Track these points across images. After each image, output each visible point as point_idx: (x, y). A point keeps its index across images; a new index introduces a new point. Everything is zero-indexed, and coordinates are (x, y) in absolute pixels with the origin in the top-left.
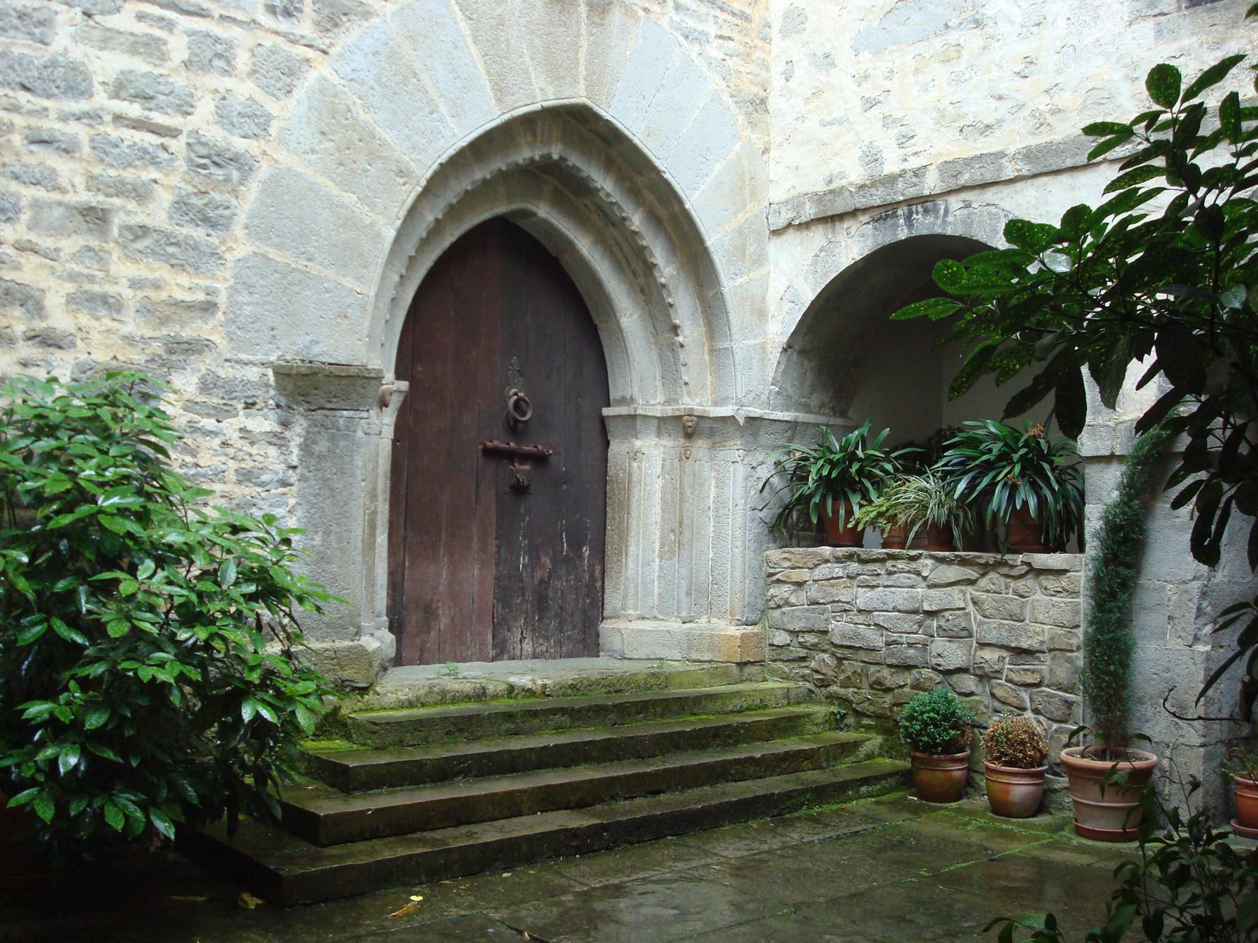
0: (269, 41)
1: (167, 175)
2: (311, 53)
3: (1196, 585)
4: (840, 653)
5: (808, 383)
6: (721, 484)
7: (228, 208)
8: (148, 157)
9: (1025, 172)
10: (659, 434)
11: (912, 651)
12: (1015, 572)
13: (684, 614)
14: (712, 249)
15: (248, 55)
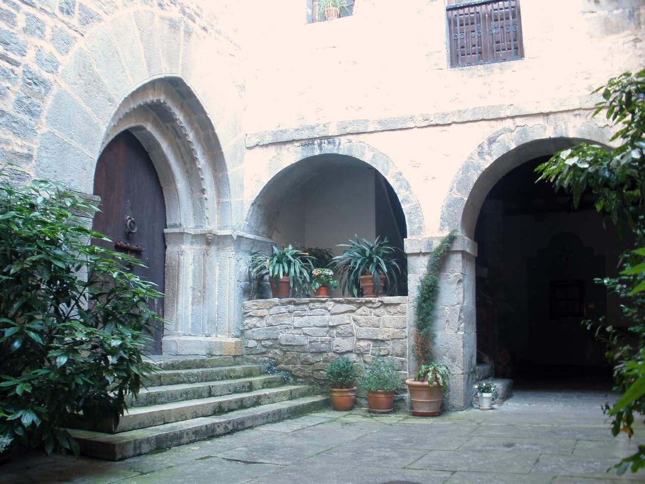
0: (60, 25)
1: (13, 86)
2: (76, 34)
3: (458, 306)
4: (285, 348)
5: (259, 221)
6: (222, 268)
7: (39, 107)
8: (6, 74)
9: (379, 129)
10: (192, 243)
11: (323, 345)
12: (375, 306)
13: (206, 332)
14: (224, 153)
15: (51, 30)
